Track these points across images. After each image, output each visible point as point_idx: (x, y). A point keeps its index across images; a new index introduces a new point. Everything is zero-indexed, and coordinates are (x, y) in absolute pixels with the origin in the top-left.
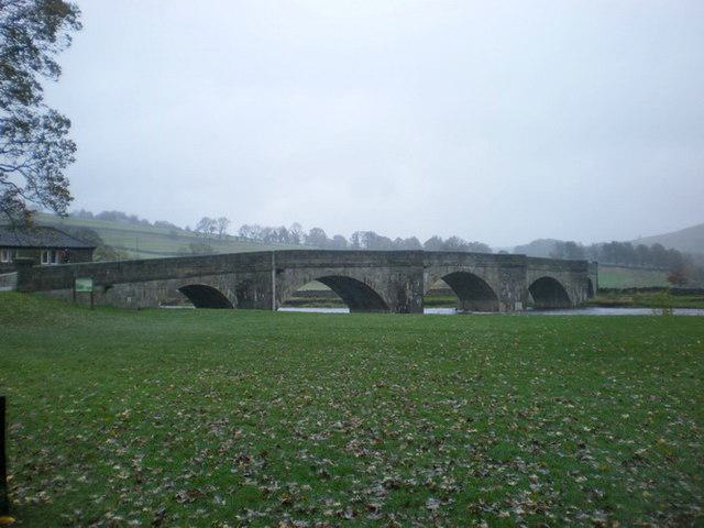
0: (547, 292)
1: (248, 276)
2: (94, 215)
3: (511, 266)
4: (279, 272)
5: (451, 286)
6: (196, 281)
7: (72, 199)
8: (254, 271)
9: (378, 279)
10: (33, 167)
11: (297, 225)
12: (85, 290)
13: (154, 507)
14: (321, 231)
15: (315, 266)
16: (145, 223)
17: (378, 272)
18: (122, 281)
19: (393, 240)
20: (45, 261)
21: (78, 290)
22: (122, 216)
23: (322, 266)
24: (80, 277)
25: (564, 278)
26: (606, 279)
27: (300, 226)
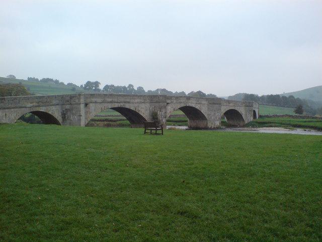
0: (232, 117)
1: (68, 107)
2: (187, 94)
3: (214, 104)
4: (86, 105)
5: (120, 113)
8: (71, 104)
9: (145, 111)
11: (130, 86)
16: (62, 84)
17: (143, 106)
19: (146, 91)
22: (51, 80)
23: (111, 102)
25: (242, 110)
26: (262, 110)
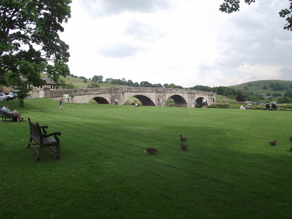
6: (97, 96)
7: (239, 10)
10: (261, 192)
12: (66, 98)
13: (61, 82)
14: (131, 81)
15: (134, 92)
18: (76, 95)
19: (153, 84)
20: (51, 88)
21: (64, 98)
23: (136, 92)
24: (64, 94)
27: (124, 79)
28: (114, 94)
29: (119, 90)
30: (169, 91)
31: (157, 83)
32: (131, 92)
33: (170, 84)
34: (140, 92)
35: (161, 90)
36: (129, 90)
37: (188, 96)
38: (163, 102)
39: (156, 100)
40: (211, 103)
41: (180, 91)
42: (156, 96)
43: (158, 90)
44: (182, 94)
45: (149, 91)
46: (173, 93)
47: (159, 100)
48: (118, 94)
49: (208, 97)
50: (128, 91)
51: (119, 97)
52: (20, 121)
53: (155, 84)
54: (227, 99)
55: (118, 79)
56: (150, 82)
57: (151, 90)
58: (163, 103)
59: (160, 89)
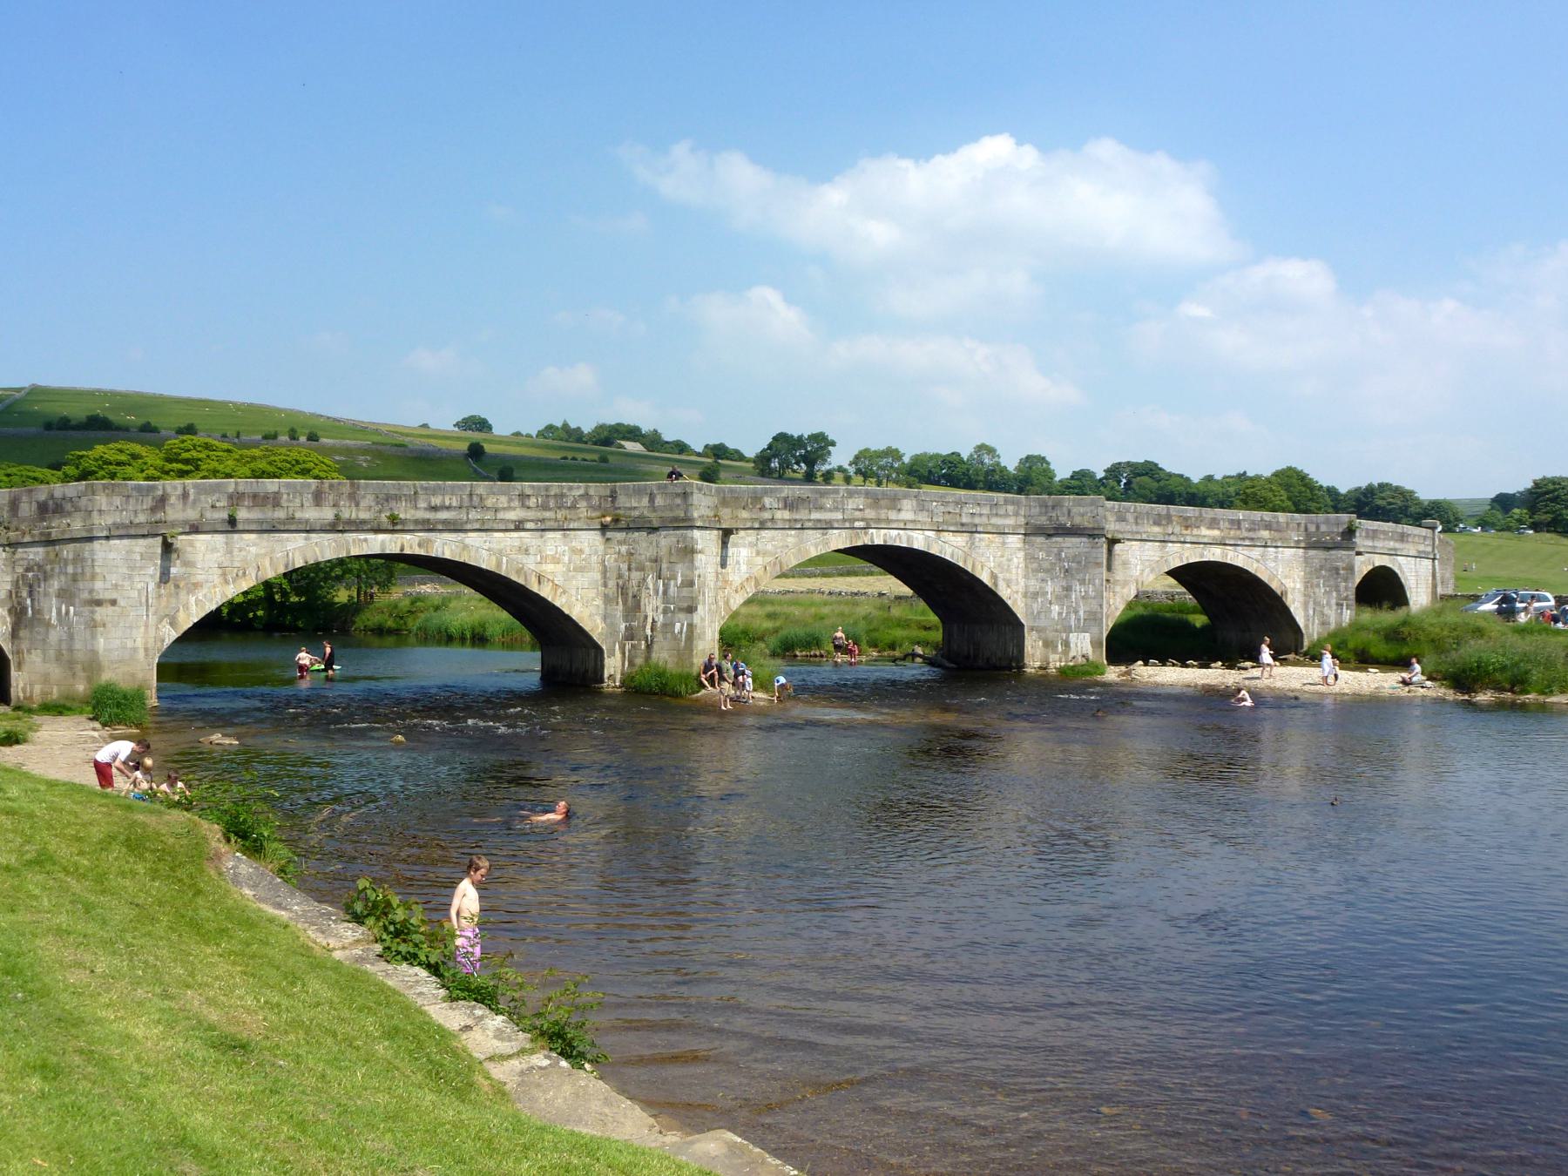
14: (1043, 460)
23: (335, 527)
27: (991, 451)
28: (37, 554)
29: (78, 509)
30: (786, 515)
31: (882, 447)
32: (272, 529)
33: (1016, 464)
34: (395, 526)
35: (645, 501)
36: (242, 514)
37: (1030, 558)
38: (665, 611)
39: (607, 600)
40: (1332, 614)
41: (921, 507)
42: (610, 560)
43: (623, 501)
44: (960, 540)
45: (512, 515)
46: (826, 526)
47: (633, 607)
48: (67, 551)
49: (1306, 560)
50: (232, 521)
51: (75, 578)
52: (1460, 532)
53: (1209, 478)
54: (1263, 737)
55: (945, 451)
56: (1169, 465)
57: (545, 507)
58: (668, 626)
59: (639, 492)
